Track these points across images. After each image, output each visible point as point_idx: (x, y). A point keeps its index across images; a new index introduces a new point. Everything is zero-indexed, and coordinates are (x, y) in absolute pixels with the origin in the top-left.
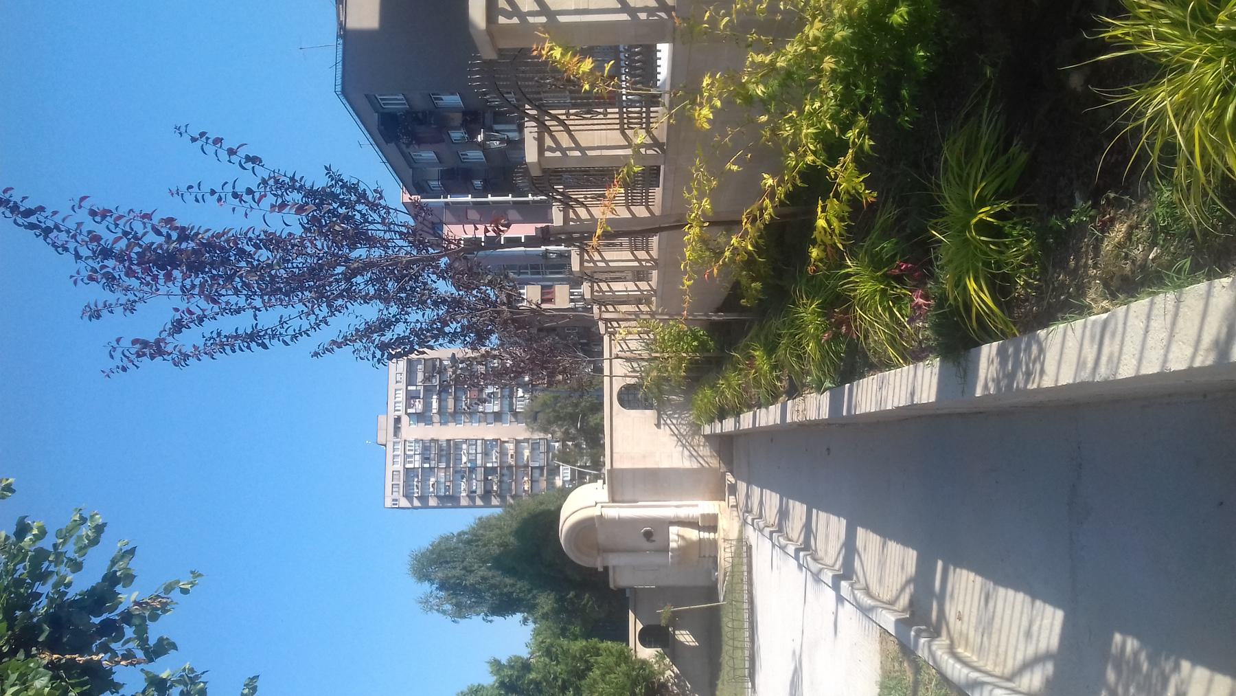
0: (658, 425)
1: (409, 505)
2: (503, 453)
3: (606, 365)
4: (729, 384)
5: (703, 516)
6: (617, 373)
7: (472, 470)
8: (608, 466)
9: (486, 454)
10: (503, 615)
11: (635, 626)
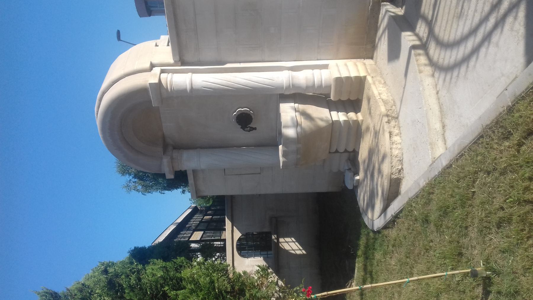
5: (339, 81)
10: (169, 190)
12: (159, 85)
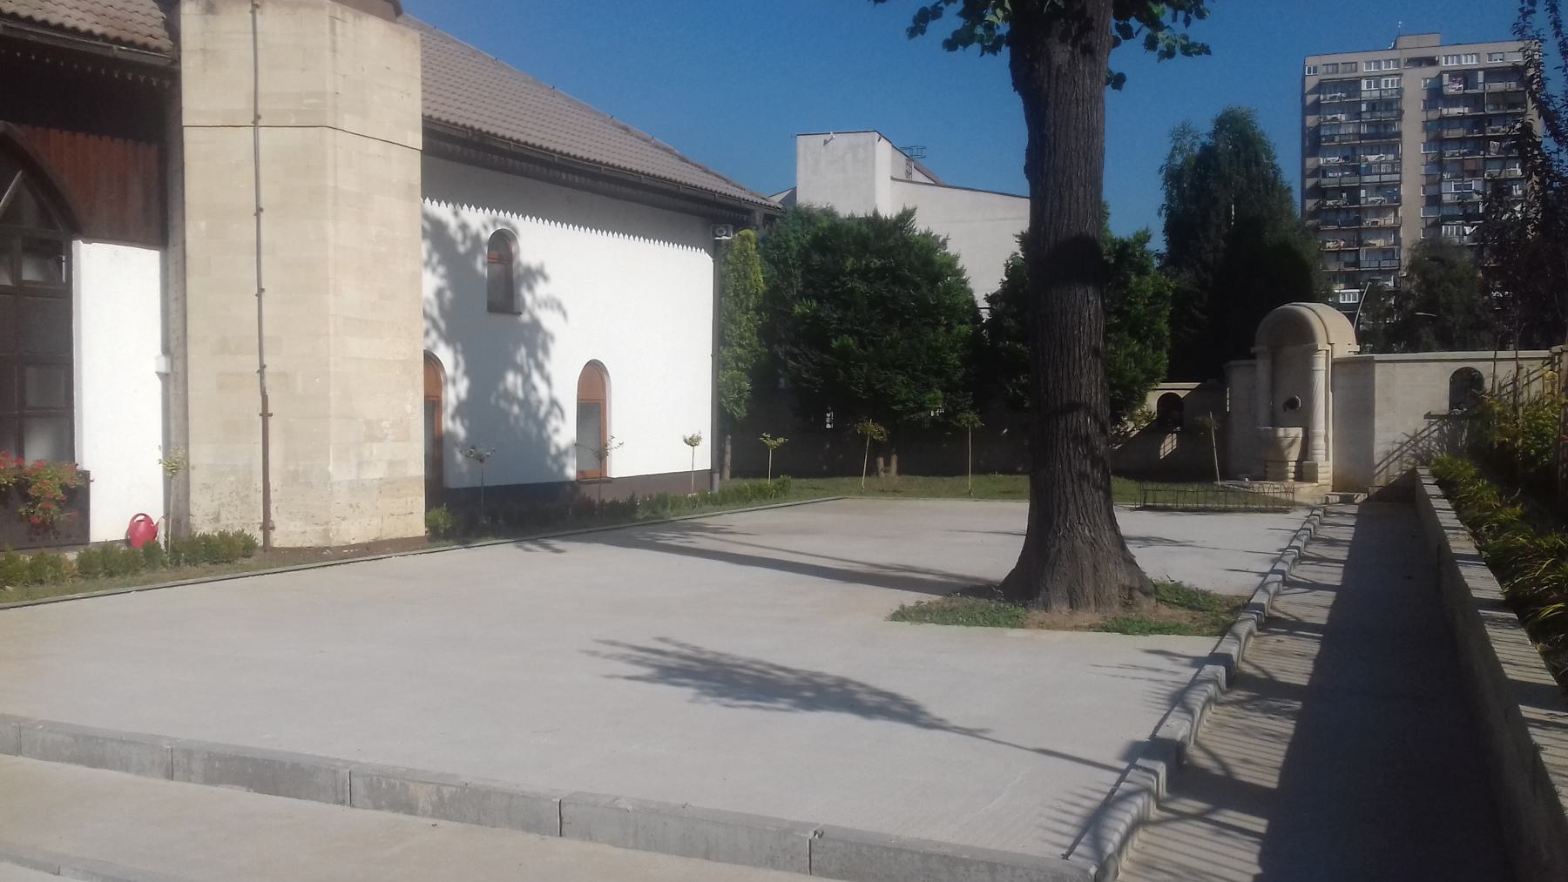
0: (1428, 416)
1: (1308, 89)
2: (1380, 210)
3: (1510, 354)
4: (1485, 491)
5: (1316, 465)
6: (1497, 368)
7: (1356, 171)
8: (1377, 357)
9: (1379, 188)
11: (1182, 389)
12: (1315, 350)
